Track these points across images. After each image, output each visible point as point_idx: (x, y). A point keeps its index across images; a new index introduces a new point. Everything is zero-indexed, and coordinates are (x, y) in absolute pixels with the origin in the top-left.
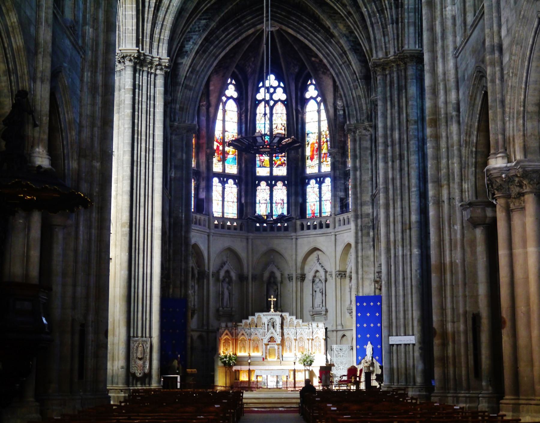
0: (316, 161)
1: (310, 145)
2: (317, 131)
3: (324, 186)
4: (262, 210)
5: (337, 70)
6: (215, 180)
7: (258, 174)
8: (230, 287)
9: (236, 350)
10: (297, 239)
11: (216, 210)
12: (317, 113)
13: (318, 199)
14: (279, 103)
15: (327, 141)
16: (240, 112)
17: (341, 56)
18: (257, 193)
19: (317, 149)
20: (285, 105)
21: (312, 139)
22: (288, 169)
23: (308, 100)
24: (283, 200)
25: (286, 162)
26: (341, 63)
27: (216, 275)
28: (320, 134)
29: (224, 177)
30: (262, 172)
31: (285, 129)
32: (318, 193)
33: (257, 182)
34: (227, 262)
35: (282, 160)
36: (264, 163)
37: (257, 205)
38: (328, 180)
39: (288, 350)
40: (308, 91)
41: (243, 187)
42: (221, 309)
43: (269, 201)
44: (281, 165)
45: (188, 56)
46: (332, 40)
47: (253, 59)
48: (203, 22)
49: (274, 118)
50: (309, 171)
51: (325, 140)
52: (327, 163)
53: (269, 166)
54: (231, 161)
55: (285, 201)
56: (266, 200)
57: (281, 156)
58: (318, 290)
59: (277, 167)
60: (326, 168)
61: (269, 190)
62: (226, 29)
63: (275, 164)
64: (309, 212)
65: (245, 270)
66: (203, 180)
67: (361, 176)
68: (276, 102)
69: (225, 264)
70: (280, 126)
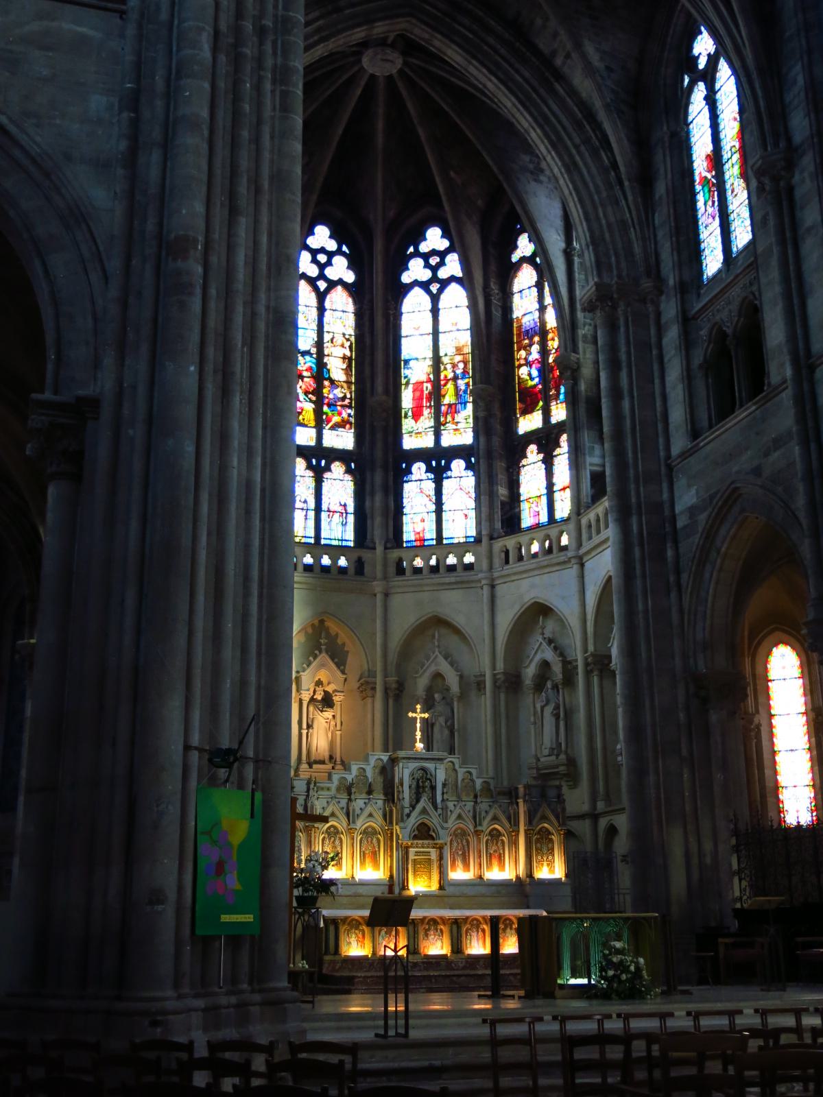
0: (427, 421)
1: (411, 387)
12: (430, 315)
13: (433, 507)
14: (339, 288)
15: (455, 378)
17: (579, 125)
21: (417, 371)
24: (345, 506)
25: (352, 420)
26: (577, 141)
28: (437, 361)
31: (350, 347)
32: (432, 493)
35: (345, 415)
36: (301, 417)
39: (459, 864)
40: (407, 269)
43: (312, 504)
44: (342, 425)
49: (326, 320)
50: (408, 443)
51: (450, 375)
52: (455, 427)
53: (313, 424)
55: (351, 509)
59: (332, 428)
60: (460, 432)
63: (329, 420)
64: (408, 535)
68: (332, 284)
70: (339, 339)
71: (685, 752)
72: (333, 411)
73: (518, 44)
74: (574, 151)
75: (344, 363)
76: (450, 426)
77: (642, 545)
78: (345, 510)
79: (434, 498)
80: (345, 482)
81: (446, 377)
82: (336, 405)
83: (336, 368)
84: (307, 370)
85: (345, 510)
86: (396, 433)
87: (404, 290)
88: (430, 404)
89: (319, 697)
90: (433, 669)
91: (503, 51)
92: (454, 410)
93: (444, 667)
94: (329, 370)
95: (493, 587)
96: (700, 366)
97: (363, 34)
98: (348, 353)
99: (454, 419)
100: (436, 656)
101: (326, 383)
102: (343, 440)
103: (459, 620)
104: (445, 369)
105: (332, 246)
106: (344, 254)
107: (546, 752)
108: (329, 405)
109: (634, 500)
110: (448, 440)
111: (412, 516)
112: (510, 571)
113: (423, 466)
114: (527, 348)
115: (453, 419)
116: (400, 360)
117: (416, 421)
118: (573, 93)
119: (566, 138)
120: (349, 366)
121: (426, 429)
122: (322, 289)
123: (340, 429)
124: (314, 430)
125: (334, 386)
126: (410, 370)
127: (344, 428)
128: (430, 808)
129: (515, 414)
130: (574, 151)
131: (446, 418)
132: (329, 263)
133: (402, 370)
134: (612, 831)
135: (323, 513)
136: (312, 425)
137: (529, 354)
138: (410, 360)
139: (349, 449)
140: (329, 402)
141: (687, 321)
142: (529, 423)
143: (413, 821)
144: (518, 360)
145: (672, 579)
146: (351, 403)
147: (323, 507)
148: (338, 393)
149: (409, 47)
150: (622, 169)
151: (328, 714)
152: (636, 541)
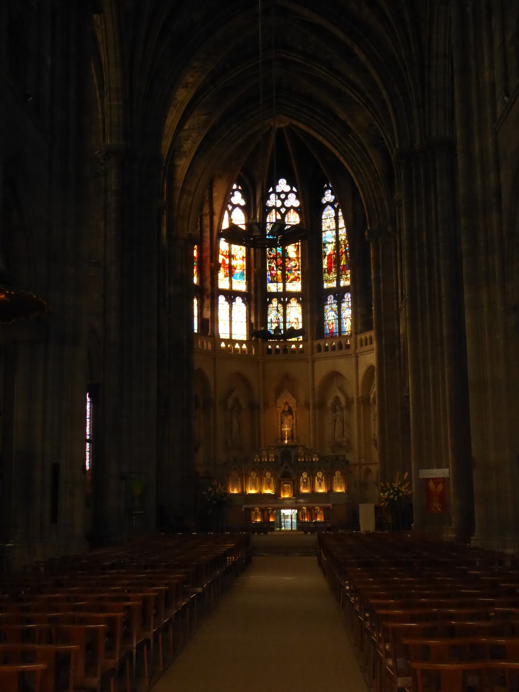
0: (333, 276)
3: (344, 305)
6: (222, 299)
7: (268, 291)
10: (313, 362)
11: (223, 332)
18: (269, 312)
19: (335, 260)
21: (329, 249)
22: (302, 284)
23: (324, 206)
24: (297, 319)
25: (300, 276)
28: (338, 243)
30: (272, 287)
35: (296, 274)
36: (275, 278)
38: (348, 296)
41: (253, 305)
44: (295, 279)
50: (326, 285)
51: (344, 250)
54: (238, 276)
57: (295, 270)
59: (291, 282)
60: (345, 283)
63: (288, 278)
66: (208, 298)
68: (288, 209)
72: (290, 273)
75: (295, 248)
76: (344, 276)
78: (298, 321)
79: (337, 312)
80: (297, 308)
82: (292, 270)
85: (298, 321)
86: (321, 282)
87: (323, 207)
88: (335, 266)
89: (286, 409)
90: (334, 395)
91: (323, 122)
92: (345, 268)
93: (339, 394)
94: (288, 253)
95: (357, 357)
99: (345, 273)
100: (336, 389)
101: (287, 260)
102: (295, 287)
103: (344, 372)
104: (342, 247)
105: (287, 188)
106: (294, 192)
108: (288, 271)
110: (343, 283)
111: (328, 321)
115: (345, 272)
116: (322, 244)
117: (329, 275)
120: (298, 249)
121: (333, 278)
122: (283, 212)
123: (294, 282)
125: (290, 260)
126: (326, 249)
127: (296, 281)
131: (342, 273)
132: (286, 198)
133: (300, 245)
134: (369, 471)
135: (287, 324)
136: (281, 282)
138: (326, 243)
139: (298, 291)
140: (288, 269)
146: (299, 268)
147: (287, 320)
148: (293, 264)
151: (290, 417)
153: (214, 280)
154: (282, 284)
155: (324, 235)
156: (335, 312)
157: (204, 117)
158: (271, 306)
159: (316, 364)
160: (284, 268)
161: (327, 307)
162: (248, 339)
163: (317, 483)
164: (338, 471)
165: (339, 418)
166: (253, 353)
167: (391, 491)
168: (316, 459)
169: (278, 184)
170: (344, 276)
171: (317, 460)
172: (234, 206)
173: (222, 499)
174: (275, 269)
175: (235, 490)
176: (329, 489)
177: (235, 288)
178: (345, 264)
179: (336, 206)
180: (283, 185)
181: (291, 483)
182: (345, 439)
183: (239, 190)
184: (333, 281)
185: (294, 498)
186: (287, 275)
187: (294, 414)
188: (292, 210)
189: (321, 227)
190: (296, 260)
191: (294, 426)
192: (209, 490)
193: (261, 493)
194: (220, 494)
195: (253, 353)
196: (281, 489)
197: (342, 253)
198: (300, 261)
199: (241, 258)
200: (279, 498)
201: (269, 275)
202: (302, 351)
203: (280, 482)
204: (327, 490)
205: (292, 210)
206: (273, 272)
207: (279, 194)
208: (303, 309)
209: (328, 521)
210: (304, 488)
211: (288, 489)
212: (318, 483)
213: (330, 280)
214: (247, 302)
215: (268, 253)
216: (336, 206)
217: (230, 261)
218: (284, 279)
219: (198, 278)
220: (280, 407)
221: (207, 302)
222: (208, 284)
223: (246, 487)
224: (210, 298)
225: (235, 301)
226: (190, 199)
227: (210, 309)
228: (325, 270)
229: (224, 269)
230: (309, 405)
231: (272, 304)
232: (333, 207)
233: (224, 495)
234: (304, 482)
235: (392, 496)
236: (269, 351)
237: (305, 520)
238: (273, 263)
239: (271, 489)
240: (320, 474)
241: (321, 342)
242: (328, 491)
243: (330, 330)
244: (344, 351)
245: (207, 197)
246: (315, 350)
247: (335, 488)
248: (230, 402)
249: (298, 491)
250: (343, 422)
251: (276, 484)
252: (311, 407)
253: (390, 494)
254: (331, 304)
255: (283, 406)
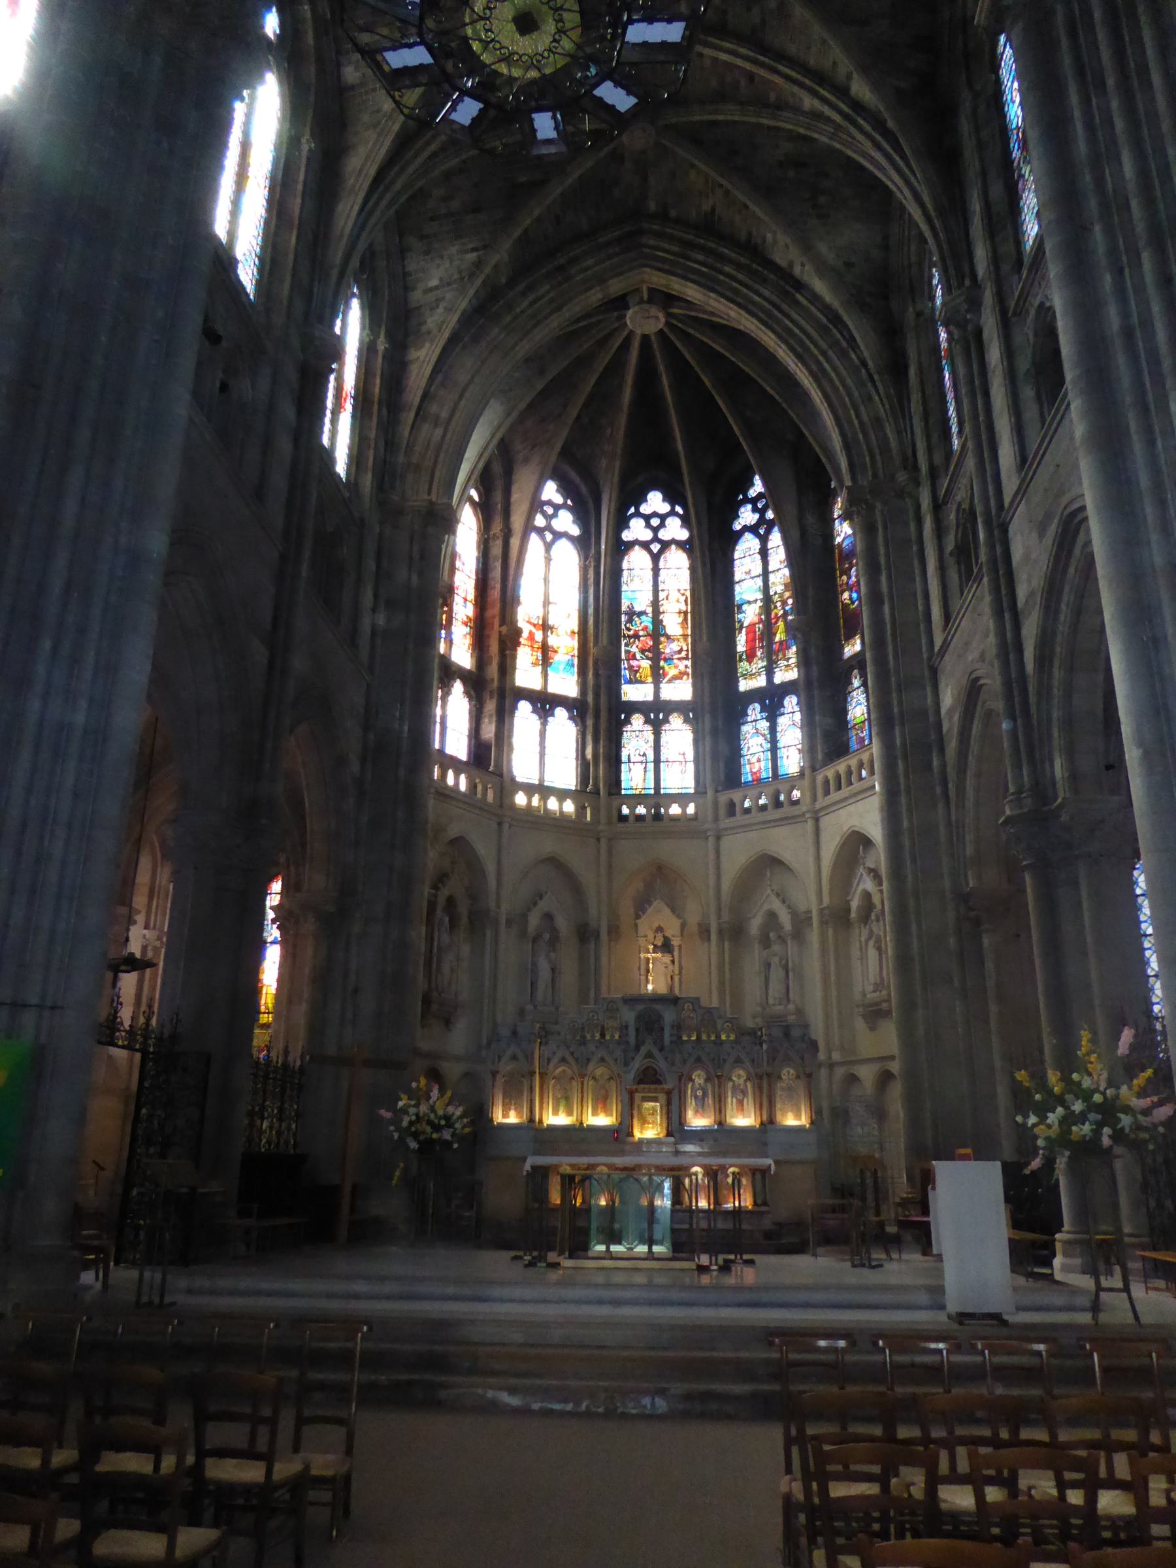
0: (759, 663)
2: (760, 596)
3: (782, 721)
4: (634, 778)
5: (814, 367)
7: (624, 699)
8: (553, 955)
9: (541, 1109)
10: (718, 838)
12: (758, 557)
14: (637, 547)
15: (785, 614)
16: (585, 565)
17: (824, 330)
18: (624, 741)
19: (762, 634)
20: (684, 550)
21: (750, 615)
22: (694, 685)
25: (690, 671)
26: (824, 346)
27: (519, 920)
28: (767, 600)
29: (545, 703)
30: (632, 693)
31: (686, 601)
33: (623, 716)
34: (546, 893)
35: (682, 668)
36: (638, 675)
37: (624, 767)
38: (791, 702)
41: (590, 722)
42: (529, 1007)
43: (651, 756)
45: (432, 341)
46: (799, 297)
47: (609, 431)
48: (472, 256)
50: (744, 685)
52: (786, 663)
54: (562, 667)
56: (644, 755)
57: (679, 659)
58: (775, 961)
59: (670, 681)
60: (786, 674)
61: (650, 733)
62: (530, 288)
63: (665, 675)
64: (747, 777)
65: (593, 912)
67: (892, 615)
68: (665, 545)
69: (541, 898)
71: (956, 984)
73: (754, 266)
74: (821, 358)
76: (782, 663)
77: (905, 757)
79: (769, 736)
81: (776, 614)
83: (673, 624)
84: (643, 630)
86: (732, 677)
90: (766, 907)
93: (776, 905)
94: (664, 627)
95: (817, 820)
96: (951, 554)
97: (600, 296)
98: (684, 608)
100: (769, 895)
101: (662, 639)
103: (786, 856)
104: (776, 607)
105: (665, 508)
106: (677, 514)
107: (871, 988)
108: (665, 660)
109: (896, 710)
110: (780, 677)
111: (748, 757)
112: (832, 801)
113: (757, 706)
114: (847, 572)
115: (784, 655)
116: (734, 606)
117: (750, 664)
118: (815, 298)
119: (812, 347)
120: (685, 619)
122: (655, 551)
124: (652, 685)
128: (655, 1052)
129: (841, 641)
130: (821, 358)
131: (778, 656)
132: (662, 525)
133: (689, 610)
134: (853, 1079)
135: (662, 764)
137: (849, 578)
141: (938, 507)
142: (853, 648)
143: (637, 1064)
144: (841, 586)
145: (938, 790)
146: (687, 655)
148: (675, 646)
149: (666, 299)
150: (870, 364)
152: (899, 753)
153: (507, 667)
154: (652, 686)
155: (737, 588)
156: (763, 735)
157: (474, 255)
158: (629, 728)
159: (726, 842)
160: (656, 656)
161: (745, 728)
162: (579, 788)
163: (731, 1102)
164: (788, 1069)
165: (776, 960)
166: (589, 819)
167: (1078, 1107)
168: (728, 1036)
169: (646, 501)
170: (782, 663)
171: (732, 1037)
172: (558, 536)
173: (435, 1136)
174: (638, 656)
175: (512, 1113)
176: (765, 1118)
177: (552, 689)
178: (783, 638)
179: (762, 531)
180: (655, 502)
181: (662, 1097)
182: (791, 1007)
183: (569, 509)
184: (759, 675)
185: (671, 1139)
186: (663, 668)
187: (676, 954)
188: (673, 547)
189: (732, 574)
190: (682, 640)
191: (676, 978)
192: (401, 1104)
193: (581, 1123)
194: (432, 1116)
195: (589, 819)
196: (635, 1113)
197: (777, 618)
198: (689, 640)
199: (569, 633)
200: (630, 1139)
201: (625, 669)
202: (695, 818)
203: (631, 1094)
204: (759, 1120)
205: (673, 547)
206: (634, 663)
207: (647, 518)
208: (696, 732)
209: (764, 1209)
210: (696, 1112)
211: (653, 1114)
212: (734, 1100)
213: (754, 674)
214: (579, 720)
215: (623, 627)
216: (762, 531)
217: (545, 637)
218: (657, 675)
219: (474, 659)
220: (646, 936)
221: (490, 706)
222: (493, 671)
223: (541, 1109)
224: (496, 697)
225: (553, 715)
226: (439, 432)
227: (494, 719)
228: (741, 657)
229: (533, 651)
230: (708, 931)
231: (631, 724)
232: (757, 535)
233: (443, 1122)
234: (696, 1097)
235: (1087, 1128)
236: (623, 819)
237: (700, 1204)
238: (634, 646)
239: (608, 1113)
240: (739, 1077)
241: (736, 795)
242: (762, 1124)
243: (753, 774)
244: (787, 810)
245: (499, 506)
246: (722, 812)
247: (783, 1115)
248: (534, 921)
249: (682, 1122)
250: (786, 969)
251: (621, 1101)
252: (714, 936)
253: (1069, 1120)
254: (756, 721)
255: (651, 936)
